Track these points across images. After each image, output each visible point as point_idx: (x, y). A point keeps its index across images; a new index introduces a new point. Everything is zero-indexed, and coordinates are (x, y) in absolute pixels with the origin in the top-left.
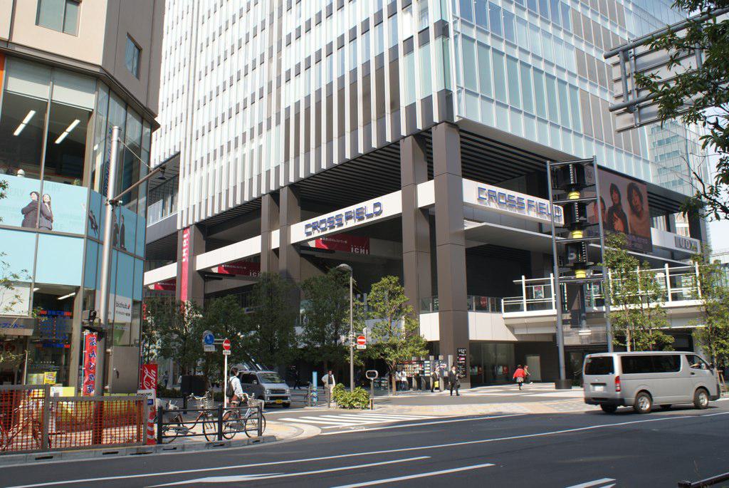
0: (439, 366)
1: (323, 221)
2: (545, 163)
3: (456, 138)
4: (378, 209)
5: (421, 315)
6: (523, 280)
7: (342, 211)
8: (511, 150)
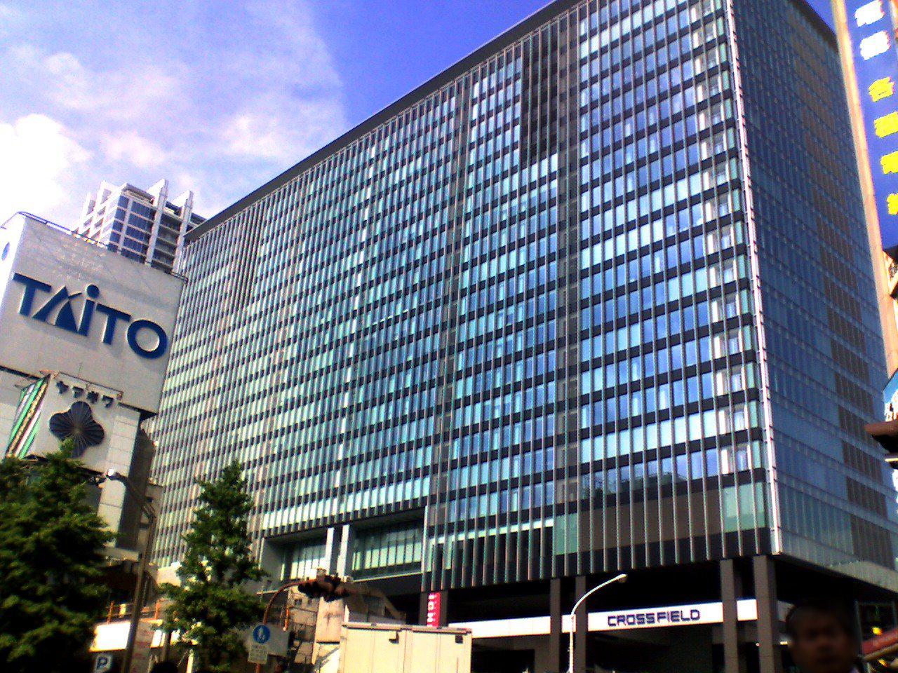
4: (695, 615)
5: (876, 121)
7: (655, 611)
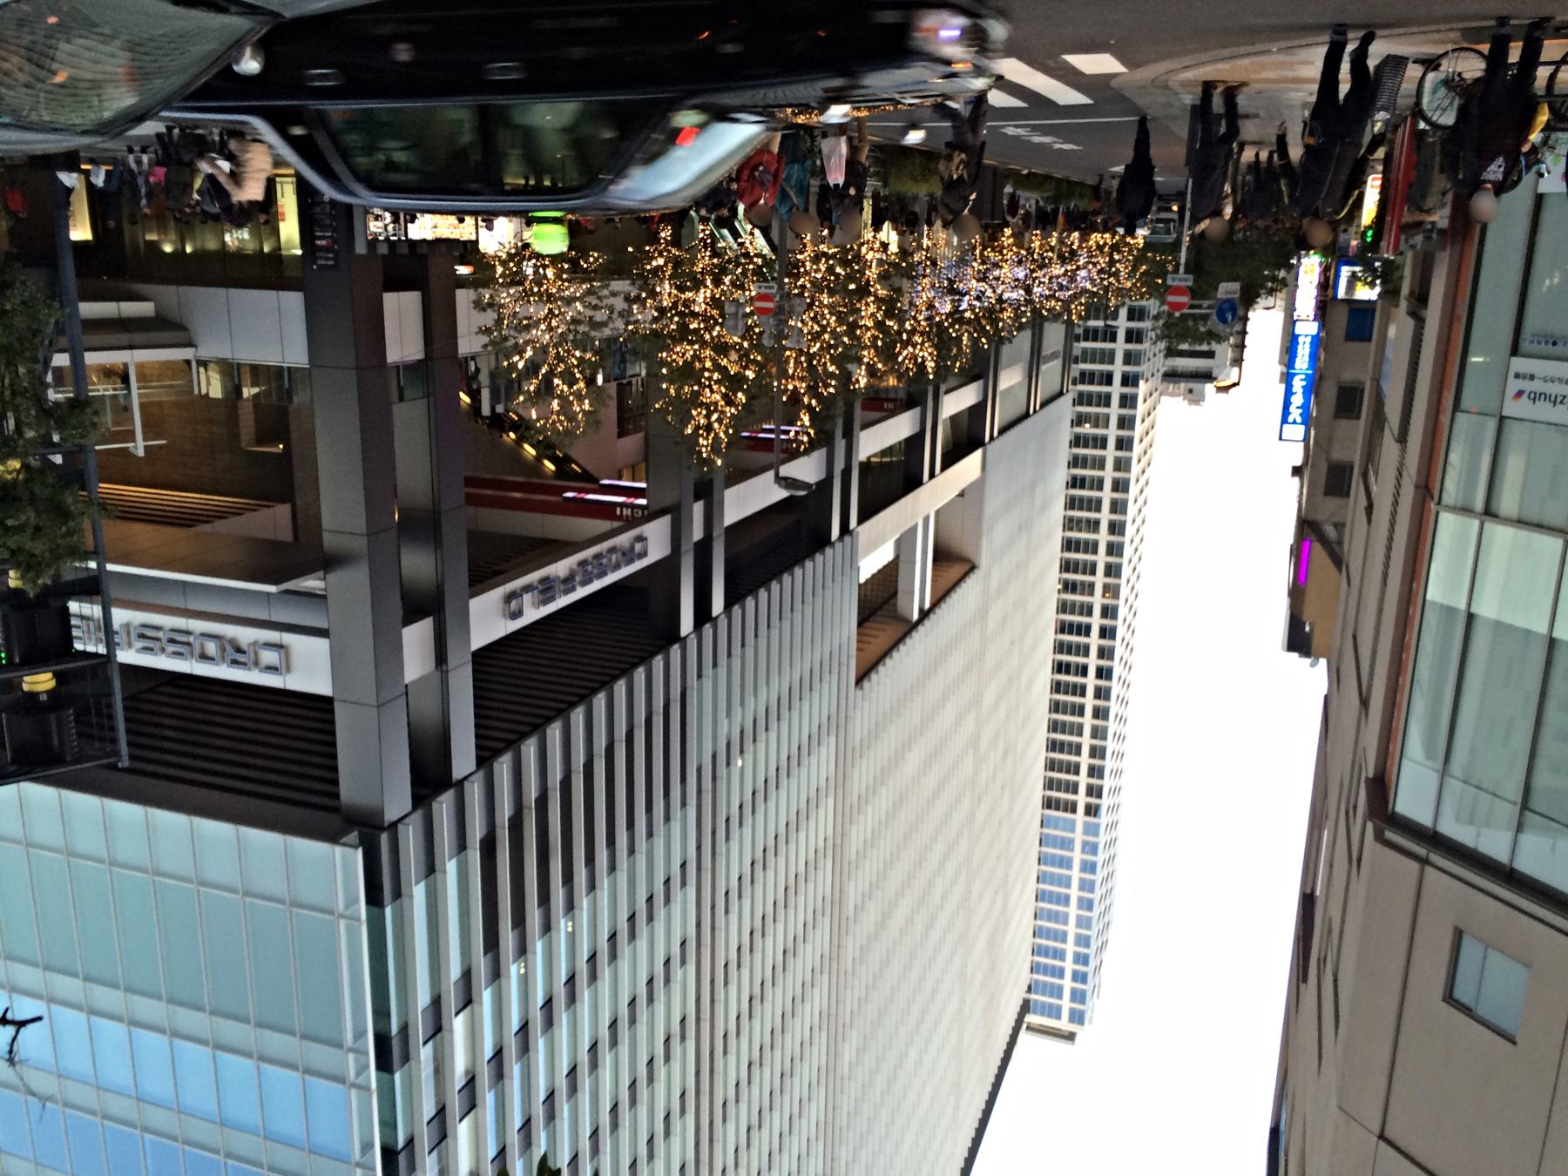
0: (386, 226)
1: (617, 567)
2: (132, 757)
3: (350, 790)
6: (139, 447)
8: (238, 784)
